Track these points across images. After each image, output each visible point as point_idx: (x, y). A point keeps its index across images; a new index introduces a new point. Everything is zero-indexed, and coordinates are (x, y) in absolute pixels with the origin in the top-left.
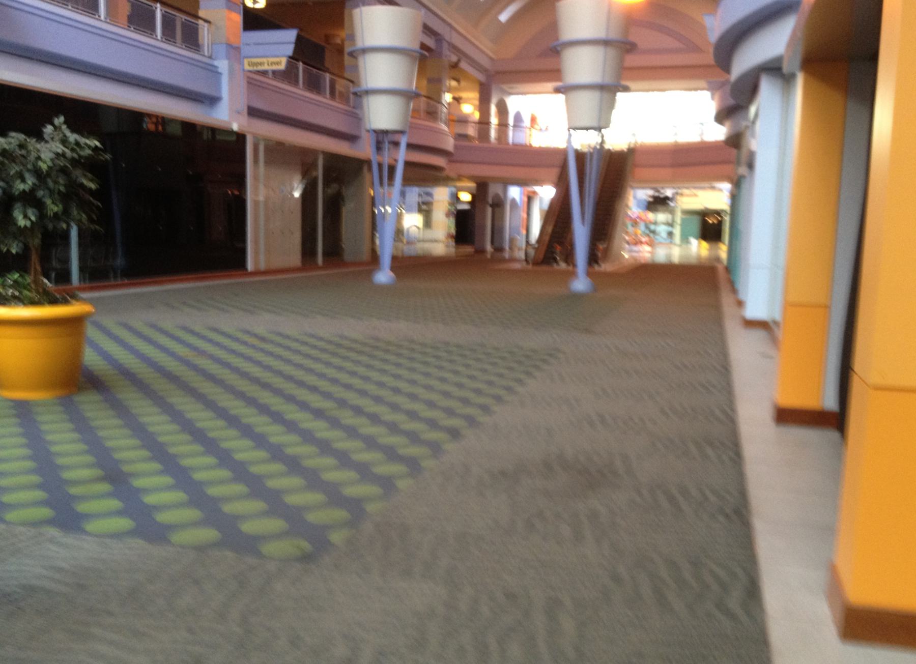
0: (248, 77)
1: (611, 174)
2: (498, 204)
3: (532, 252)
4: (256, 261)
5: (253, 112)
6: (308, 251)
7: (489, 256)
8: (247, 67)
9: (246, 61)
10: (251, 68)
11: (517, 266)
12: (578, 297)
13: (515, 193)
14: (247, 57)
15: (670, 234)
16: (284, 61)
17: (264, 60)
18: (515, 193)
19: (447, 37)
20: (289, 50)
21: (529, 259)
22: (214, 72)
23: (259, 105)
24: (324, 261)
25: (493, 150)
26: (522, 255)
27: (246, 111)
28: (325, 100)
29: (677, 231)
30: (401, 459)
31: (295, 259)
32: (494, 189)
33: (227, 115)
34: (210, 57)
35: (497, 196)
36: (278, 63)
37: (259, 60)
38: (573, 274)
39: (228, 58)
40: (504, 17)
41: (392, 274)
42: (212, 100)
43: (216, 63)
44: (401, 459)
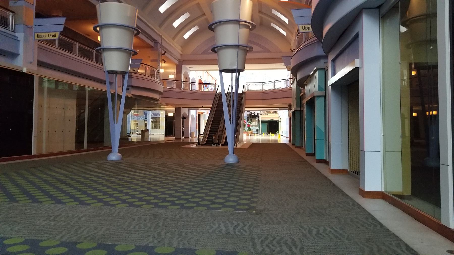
0: (38, 45)
1: (239, 100)
2: (185, 118)
3: (201, 138)
4: (39, 147)
5: (41, 64)
6: (79, 142)
7: (181, 141)
8: (36, 38)
9: (36, 34)
10: (39, 38)
11: (195, 146)
12: (231, 165)
13: (193, 113)
14: (36, 33)
15: (257, 130)
16: (58, 34)
17: (47, 34)
18: (193, 113)
19: (160, 42)
20: (61, 29)
21: (201, 143)
22: (16, 40)
23: (45, 59)
24: (87, 147)
25: (183, 93)
26: (196, 140)
27: (36, 63)
28: (93, 63)
29: (260, 129)
30: (168, 201)
31: (71, 145)
32: (184, 111)
33: (23, 63)
34: (14, 32)
35: (185, 113)
36: (54, 36)
37: (43, 34)
38: (226, 152)
39: (24, 32)
40: (186, 36)
41: (119, 154)
42: (14, 56)
43: (16, 35)
44: (168, 201)
